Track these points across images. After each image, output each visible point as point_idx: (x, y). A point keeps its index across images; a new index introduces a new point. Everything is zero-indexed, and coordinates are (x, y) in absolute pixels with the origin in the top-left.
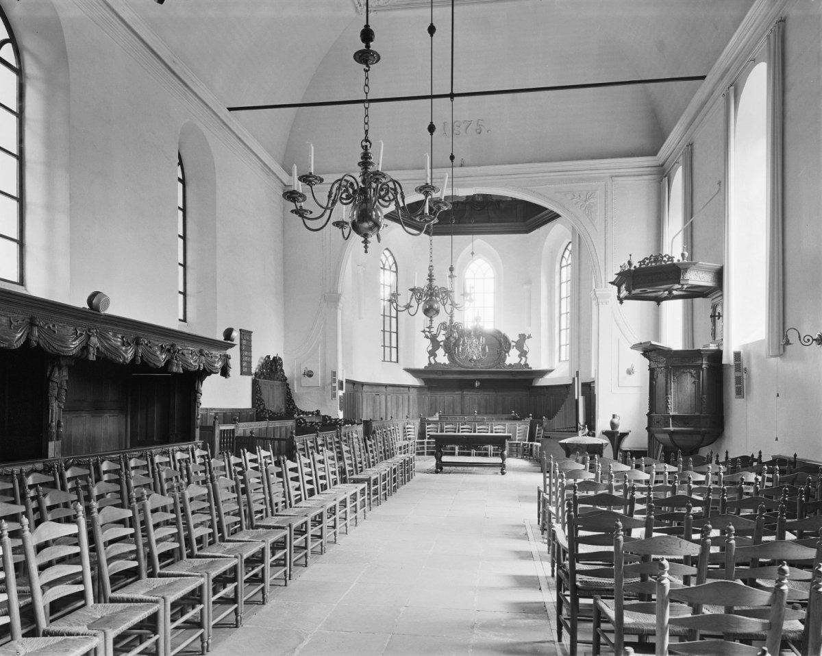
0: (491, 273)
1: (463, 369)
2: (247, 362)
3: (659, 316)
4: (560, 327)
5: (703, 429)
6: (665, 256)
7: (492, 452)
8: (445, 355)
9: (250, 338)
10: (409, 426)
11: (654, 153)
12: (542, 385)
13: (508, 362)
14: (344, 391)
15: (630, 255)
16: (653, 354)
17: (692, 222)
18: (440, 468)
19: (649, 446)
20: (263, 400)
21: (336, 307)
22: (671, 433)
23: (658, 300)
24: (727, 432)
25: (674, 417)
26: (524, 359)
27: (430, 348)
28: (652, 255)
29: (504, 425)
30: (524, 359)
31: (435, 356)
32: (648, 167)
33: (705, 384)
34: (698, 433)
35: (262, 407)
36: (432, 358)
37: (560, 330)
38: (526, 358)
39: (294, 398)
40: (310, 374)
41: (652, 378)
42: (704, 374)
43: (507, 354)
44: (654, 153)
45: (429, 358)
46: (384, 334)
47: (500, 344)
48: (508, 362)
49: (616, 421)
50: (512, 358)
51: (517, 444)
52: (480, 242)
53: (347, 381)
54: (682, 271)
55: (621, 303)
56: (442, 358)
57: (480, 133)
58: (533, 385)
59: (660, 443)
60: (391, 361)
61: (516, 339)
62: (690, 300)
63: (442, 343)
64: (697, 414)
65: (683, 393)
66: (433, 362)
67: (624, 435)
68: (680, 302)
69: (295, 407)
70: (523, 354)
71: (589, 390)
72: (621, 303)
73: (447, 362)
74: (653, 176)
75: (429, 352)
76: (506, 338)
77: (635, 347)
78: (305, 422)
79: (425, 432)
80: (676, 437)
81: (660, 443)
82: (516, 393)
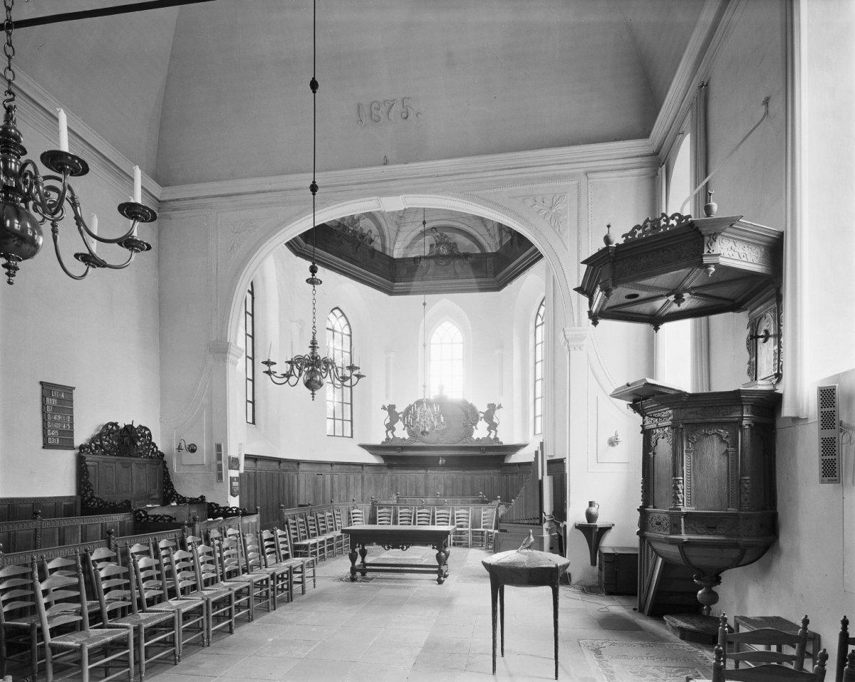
0: (459, 337)
1: (424, 444)
2: (61, 432)
3: (653, 345)
4: (535, 396)
5: (745, 539)
6: (673, 217)
7: (452, 541)
8: (404, 429)
9: (72, 398)
10: (355, 511)
11: (645, 134)
12: (515, 462)
13: (475, 436)
14: (242, 470)
15: (609, 226)
16: (648, 405)
17: (707, 184)
18: (359, 573)
19: (641, 545)
20: (91, 485)
21: (225, 360)
22: (683, 545)
23: (656, 320)
24: (784, 540)
25: (687, 516)
26: (493, 432)
27: (388, 421)
28: (647, 220)
29: (468, 509)
30: (493, 432)
31: (394, 429)
32: (637, 157)
33: (748, 455)
34: (736, 546)
35: (169, 491)
36: (389, 433)
37: (535, 399)
38: (496, 431)
39: (173, 480)
40: (192, 449)
41: (648, 447)
42: (744, 438)
43: (474, 427)
44: (645, 134)
45: (387, 432)
46: (343, 406)
47: (470, 416)
48: (475, 436)
49: (593, 510)
50: (480, 432)
51: (483, 532)
52: (444, 302)
53: (247, 457)
54: (707, 239)
55: (595, 323)
56: (401, 433)
57: (406, 118)
58: (506, 462)
59: (658, 555)
60: (343, 436)
61: (485, 409)
62: (704, 319)
63: (401, 416)
64: (732, 510)
65: (707, 470)
66: (391, 437)
67: (604, 530)
68: (687, 324)
69: (174, 492)
70: (493, 426)
71: (557, 467)
72: (595, 323)
73: (407, 437)
74: (645, 169)
75: (387, 426)
76: (473, 409)
77: (618, 395)
78: (147, 516)
79: (376, 516)
80: (692, 553)
81: (658, 555)
82: (486, 471)
